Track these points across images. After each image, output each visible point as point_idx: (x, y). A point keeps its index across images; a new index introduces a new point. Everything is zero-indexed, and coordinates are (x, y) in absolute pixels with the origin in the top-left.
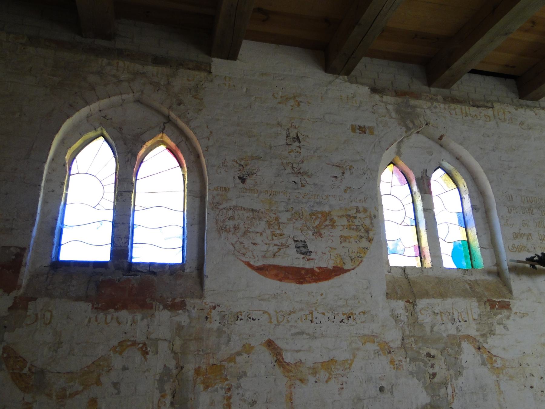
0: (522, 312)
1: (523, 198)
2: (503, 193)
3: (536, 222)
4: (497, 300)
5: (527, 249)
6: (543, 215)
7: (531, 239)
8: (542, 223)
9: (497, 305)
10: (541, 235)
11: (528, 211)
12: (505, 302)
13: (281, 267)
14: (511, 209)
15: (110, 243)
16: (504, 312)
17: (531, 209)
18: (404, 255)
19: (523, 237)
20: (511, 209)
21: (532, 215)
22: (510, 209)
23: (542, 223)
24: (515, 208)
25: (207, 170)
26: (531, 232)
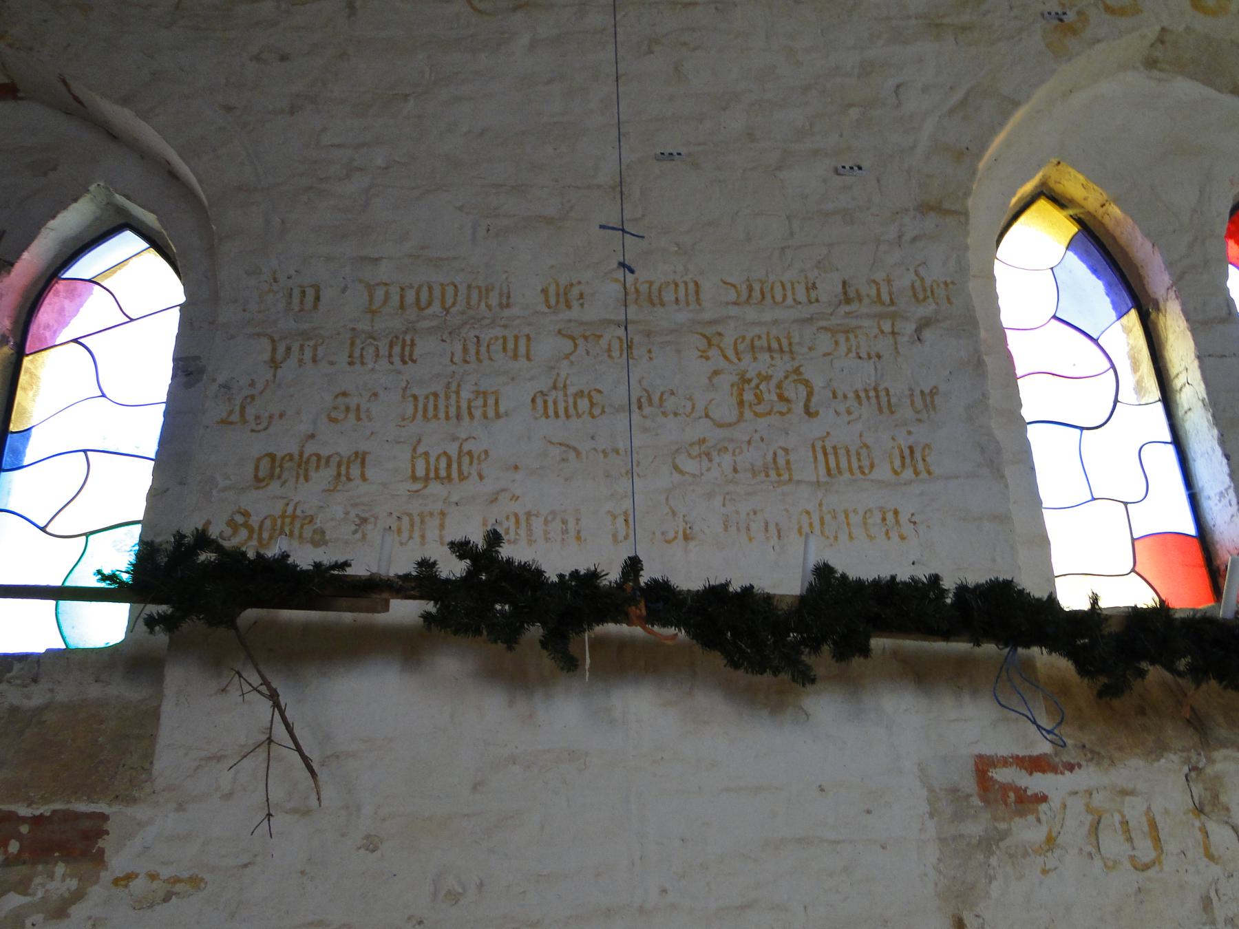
0: (166, 872)
1: (380, 293)
2: (275, 280)
3: (415, 398)
4: (23, 811)
5: (315, 531)
6: (466, 362)
7: (358, 481)
8: (454, 396)
9: (19, 837)
10: (426, 454)
11: (384, 351)
12: (77, 816)
13: (1222, 435)
14: (289, 349)
15: (165, 400)
16: (51, 876)
17: (408, 338)
18: (84, 537)
19: (312, 474)
20: (289, 349)
21: (404, 362)
22: (281, 349)
23: (454, 396)
24: (312, 343)
25: (192, 170)
26: (363, 447)
